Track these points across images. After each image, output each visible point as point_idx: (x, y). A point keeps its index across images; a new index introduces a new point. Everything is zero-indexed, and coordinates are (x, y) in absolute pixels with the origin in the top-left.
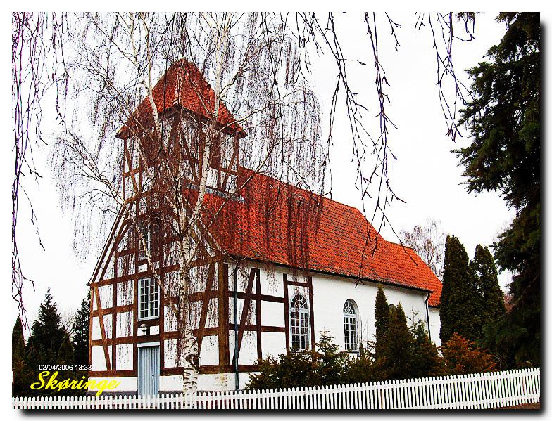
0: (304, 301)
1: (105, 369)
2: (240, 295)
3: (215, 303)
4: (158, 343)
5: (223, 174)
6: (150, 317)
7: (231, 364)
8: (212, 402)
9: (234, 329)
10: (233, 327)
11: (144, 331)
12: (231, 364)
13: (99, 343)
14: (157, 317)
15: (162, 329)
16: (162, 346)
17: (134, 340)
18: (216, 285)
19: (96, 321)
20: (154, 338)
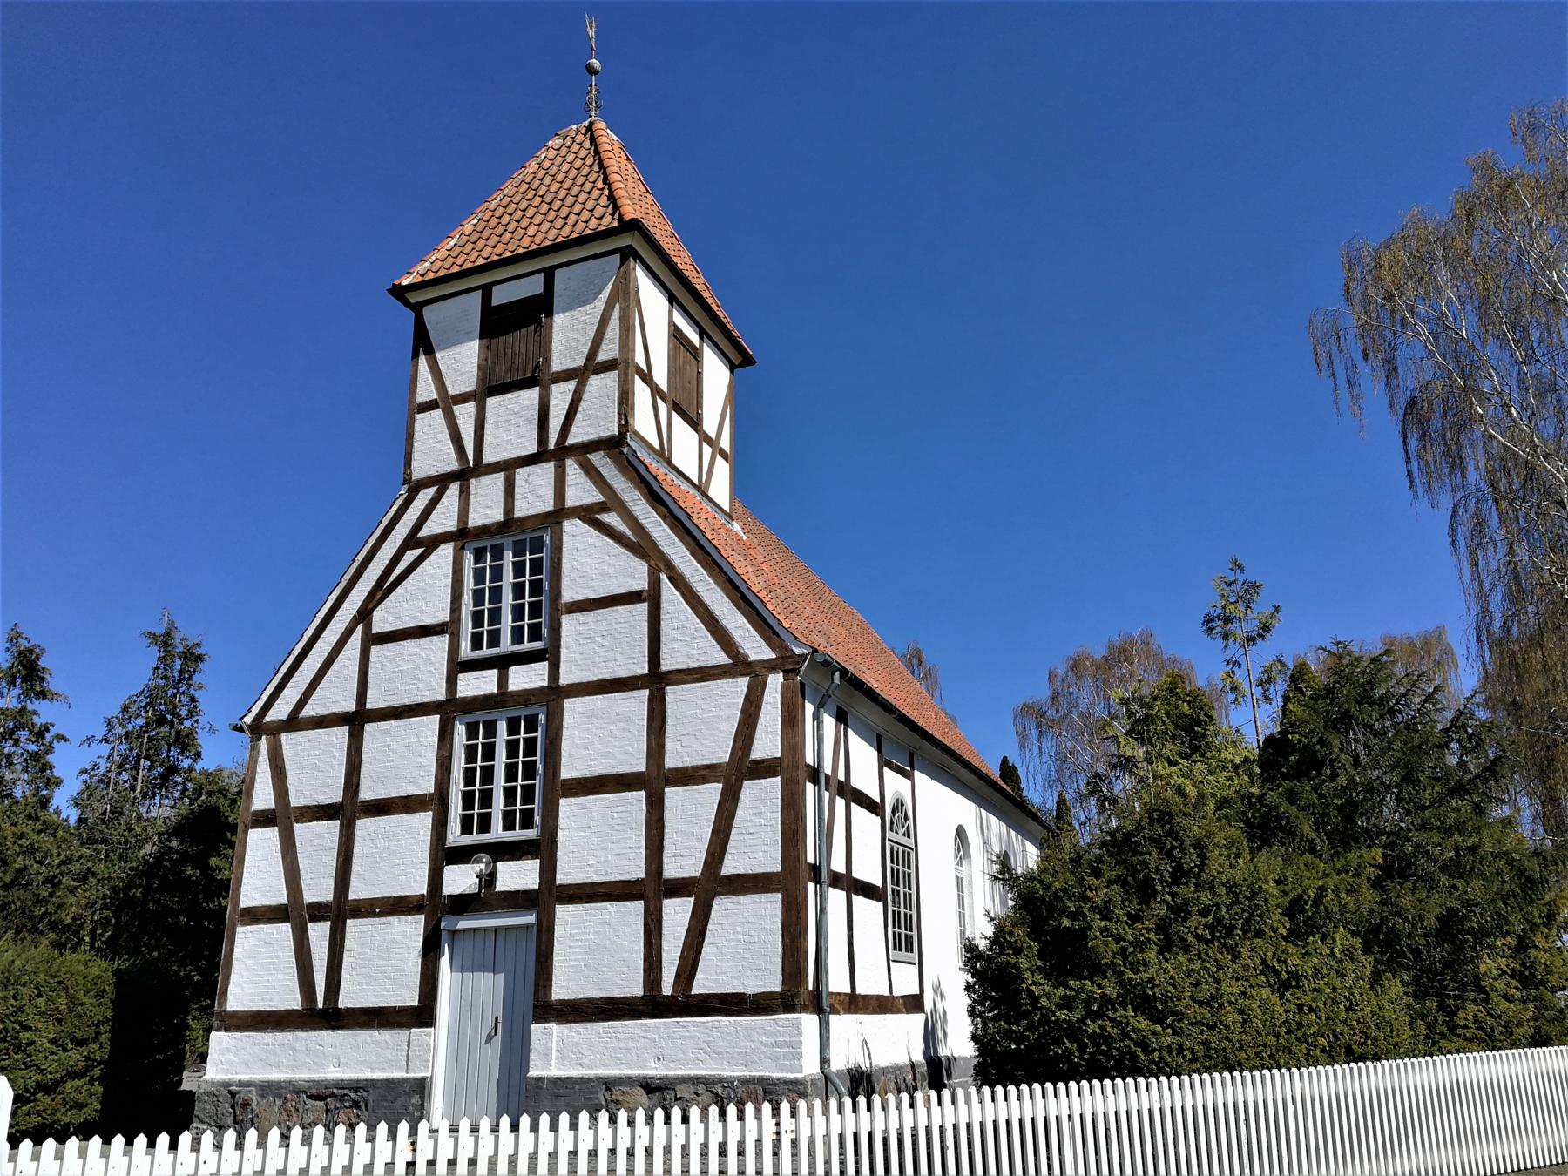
1: (294, 1002)
4: (530, 919)
6: (498, 833)
13: (295, 913)
14: (531, 834)
15: (548, 870)
16: (544, 934)
17: (436, 907)
20: (518, 901)
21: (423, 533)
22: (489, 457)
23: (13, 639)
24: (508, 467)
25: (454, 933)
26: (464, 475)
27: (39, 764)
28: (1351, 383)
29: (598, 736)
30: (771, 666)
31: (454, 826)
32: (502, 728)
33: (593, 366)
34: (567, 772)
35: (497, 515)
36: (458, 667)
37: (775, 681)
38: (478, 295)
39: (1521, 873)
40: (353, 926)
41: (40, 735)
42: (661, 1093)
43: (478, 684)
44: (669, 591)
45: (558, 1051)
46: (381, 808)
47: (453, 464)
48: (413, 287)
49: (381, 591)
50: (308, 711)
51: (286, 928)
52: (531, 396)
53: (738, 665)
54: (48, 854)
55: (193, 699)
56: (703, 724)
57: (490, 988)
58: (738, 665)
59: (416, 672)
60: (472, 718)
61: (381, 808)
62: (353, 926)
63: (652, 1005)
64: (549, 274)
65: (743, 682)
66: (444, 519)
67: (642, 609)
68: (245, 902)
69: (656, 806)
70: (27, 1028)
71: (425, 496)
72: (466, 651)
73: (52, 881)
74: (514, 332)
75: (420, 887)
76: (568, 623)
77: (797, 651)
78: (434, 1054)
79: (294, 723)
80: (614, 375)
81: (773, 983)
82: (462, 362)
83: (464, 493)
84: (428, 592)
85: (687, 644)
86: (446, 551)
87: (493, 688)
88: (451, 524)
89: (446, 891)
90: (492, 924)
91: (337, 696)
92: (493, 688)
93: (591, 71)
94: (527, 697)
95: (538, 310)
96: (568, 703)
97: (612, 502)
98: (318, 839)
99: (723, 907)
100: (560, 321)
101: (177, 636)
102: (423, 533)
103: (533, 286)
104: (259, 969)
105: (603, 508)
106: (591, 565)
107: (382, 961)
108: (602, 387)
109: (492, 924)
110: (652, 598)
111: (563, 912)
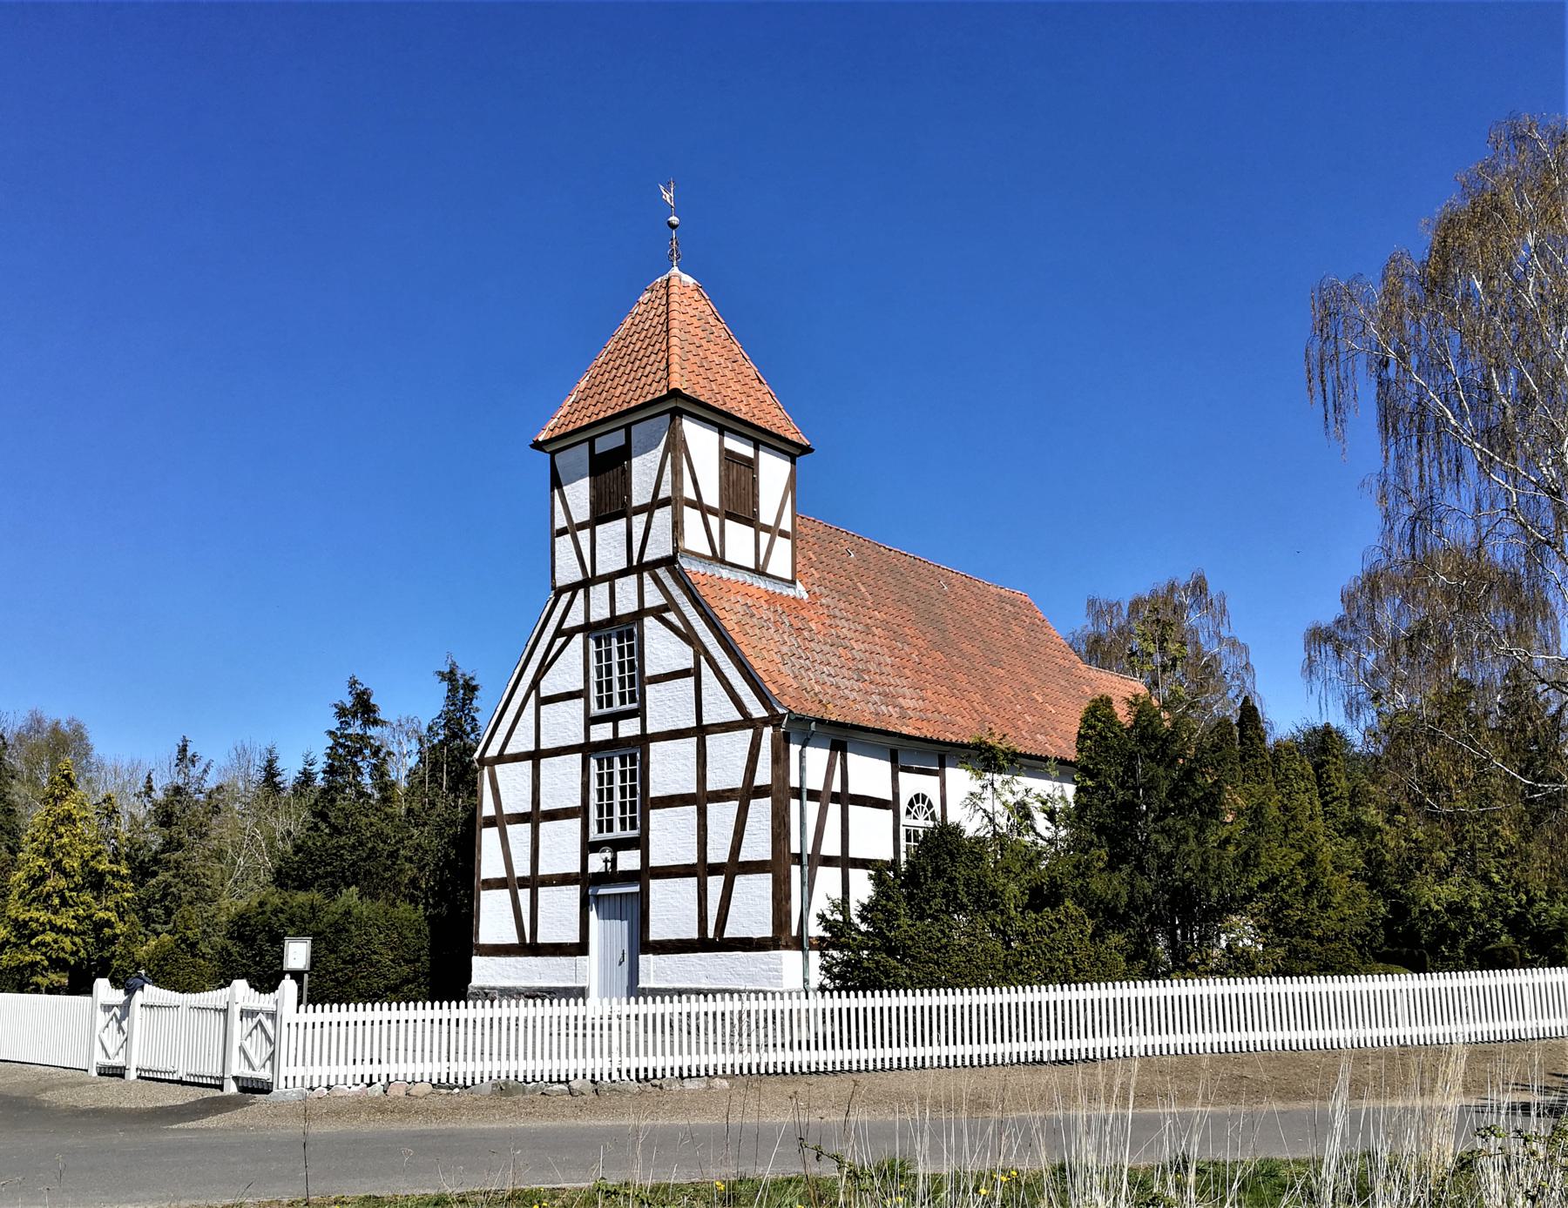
0: (930, 806)
1: (515, 940)
2: (813, 795)
3: (761, 809)
4: (636, 889)
5: (765, 537)
6: (617, 832)
7: (794, 933)
8: (646, 1016)
9: (800, 863)
10: (798, 858)
11: (606, 861)
12: (794, 933)
13: (508, 883)
15: (645, 858)
16: (644, 895)
17: (584, 880)
18: (763, 776)
19: (489, 837)
20: (629, 877)
21: (565, 626)
22: (599, 572)
23: (353, 683)
24: (611, 578)
25: (598, 898)
26: (587, 583)
27: (379, 771)
28: (1337, 407)
29: (670, 769)
30: (764, 722)
31: (593, 828)
32: (617, 761)
33: (656, 503)
34: (654, 793)
35: (607, 615)
36: (590, 721)
37: (768, 732)
38: (586, 444)
39: (1205, 861)
40: (543, 892)
41: (376, 753)
42: (534, 994)
43: (602, 732)
44: (706, 669)
45: (654, 970)
46: (553, 815)
47: (580, 577)
48: (546, 442)
49: (544, 668)
50: (508, 751)
51: (506, 892)
52: (623, 522)
53: (747, 721)
54: (388, 836)
55: (474, 719)
56: (728, 760)
57: (620, 930)
58: (747, 721)
59: (564, 724)
60: (600, 755)
61: (553, 815)
62: (543, 892)
63: (701, 944)
64: (628, 428)
65: (750, 732)
66: (575, 618)
67: (691, 681)
68: (483, 877)
69: (702, 815)
70: (375, 953)
71: (565, 597)
72: (595, 710)
73: (393, 855)
74: (610, 470)
75: (577, 869)
76: (650, 690)
77: (781, 711)
78: (589, 970)
79: (502, 758)
80: (669, 508)
81: (767, 932)
82: (579, 494)
83: (587, 596)
84: (568, 672)
85: (719, 709)
86: (579, 638)
87: (610, 736)
88: (580, 621)
89: (590, 870)
90: (616, 892)
91: (522, 741)
92: (610, 736)
93: (673, 227)
94: (630, 741)
95: (623, 454)
96: (652, 746)
97: (671, 605)
98: (519, 834)
99: (740, 881)
100: (636, 462)
101: (459, 673)
102: (565, 626)
103: (618, 439)
104: (495, 918)
105: (665, 608)
106: (662, 649)
107: (559, 913)
108: (663, 516)
109: (616, 892)
110: (695, 673)
111: (654, 885)
